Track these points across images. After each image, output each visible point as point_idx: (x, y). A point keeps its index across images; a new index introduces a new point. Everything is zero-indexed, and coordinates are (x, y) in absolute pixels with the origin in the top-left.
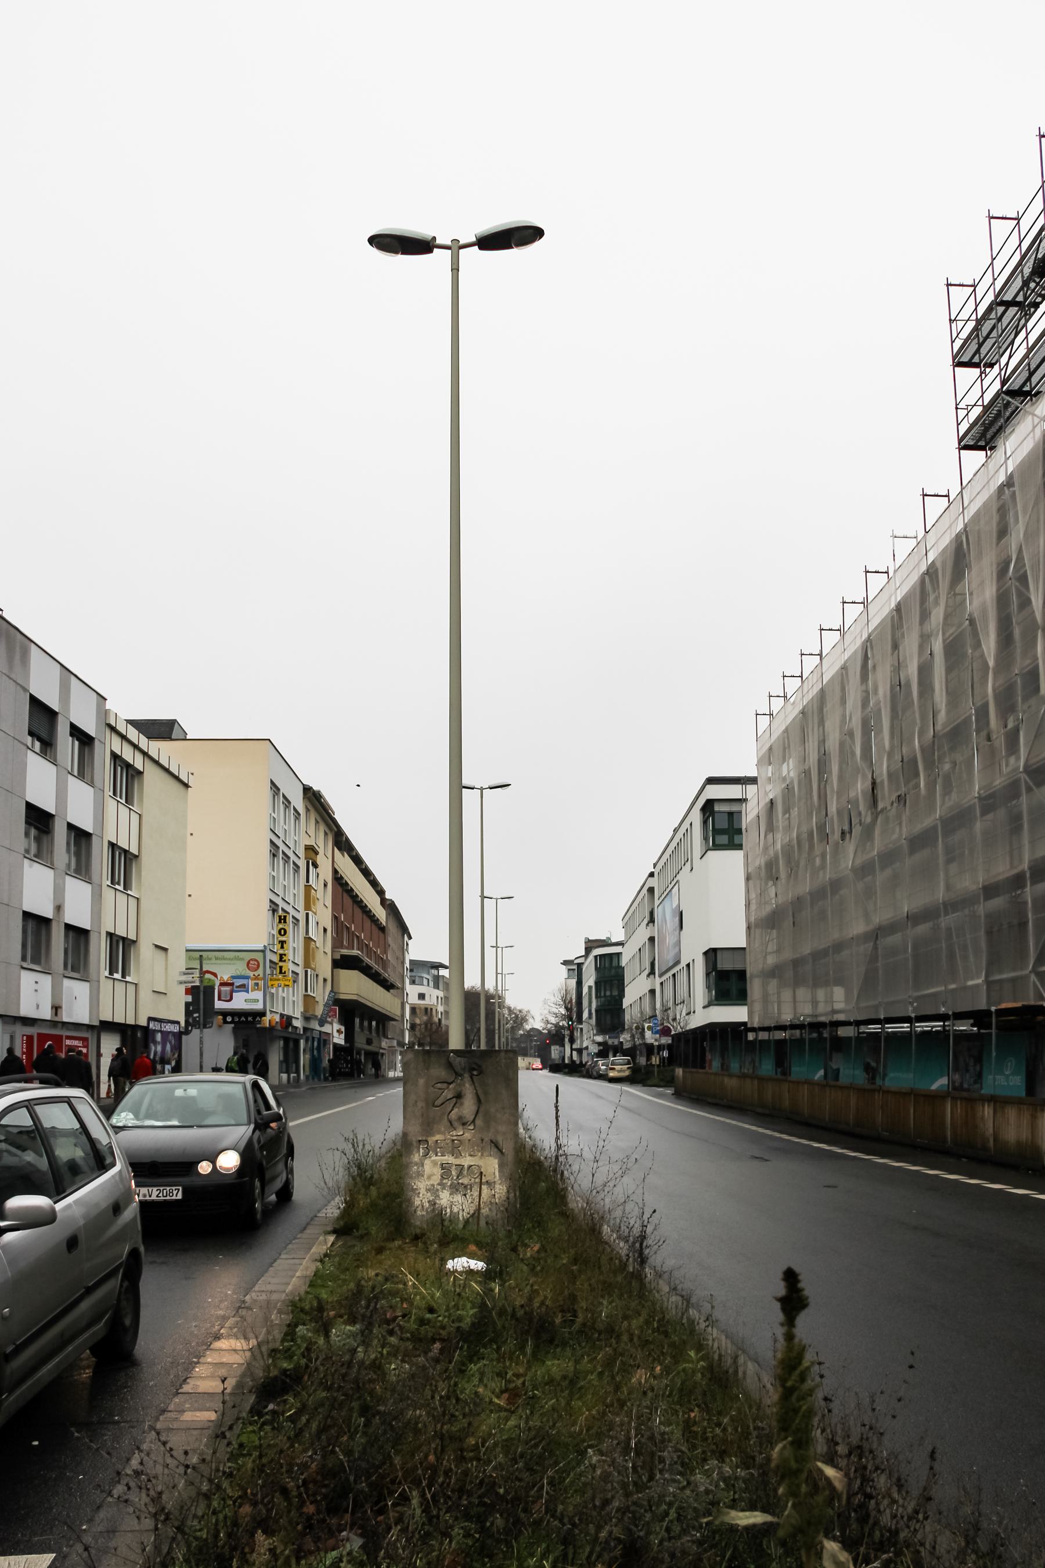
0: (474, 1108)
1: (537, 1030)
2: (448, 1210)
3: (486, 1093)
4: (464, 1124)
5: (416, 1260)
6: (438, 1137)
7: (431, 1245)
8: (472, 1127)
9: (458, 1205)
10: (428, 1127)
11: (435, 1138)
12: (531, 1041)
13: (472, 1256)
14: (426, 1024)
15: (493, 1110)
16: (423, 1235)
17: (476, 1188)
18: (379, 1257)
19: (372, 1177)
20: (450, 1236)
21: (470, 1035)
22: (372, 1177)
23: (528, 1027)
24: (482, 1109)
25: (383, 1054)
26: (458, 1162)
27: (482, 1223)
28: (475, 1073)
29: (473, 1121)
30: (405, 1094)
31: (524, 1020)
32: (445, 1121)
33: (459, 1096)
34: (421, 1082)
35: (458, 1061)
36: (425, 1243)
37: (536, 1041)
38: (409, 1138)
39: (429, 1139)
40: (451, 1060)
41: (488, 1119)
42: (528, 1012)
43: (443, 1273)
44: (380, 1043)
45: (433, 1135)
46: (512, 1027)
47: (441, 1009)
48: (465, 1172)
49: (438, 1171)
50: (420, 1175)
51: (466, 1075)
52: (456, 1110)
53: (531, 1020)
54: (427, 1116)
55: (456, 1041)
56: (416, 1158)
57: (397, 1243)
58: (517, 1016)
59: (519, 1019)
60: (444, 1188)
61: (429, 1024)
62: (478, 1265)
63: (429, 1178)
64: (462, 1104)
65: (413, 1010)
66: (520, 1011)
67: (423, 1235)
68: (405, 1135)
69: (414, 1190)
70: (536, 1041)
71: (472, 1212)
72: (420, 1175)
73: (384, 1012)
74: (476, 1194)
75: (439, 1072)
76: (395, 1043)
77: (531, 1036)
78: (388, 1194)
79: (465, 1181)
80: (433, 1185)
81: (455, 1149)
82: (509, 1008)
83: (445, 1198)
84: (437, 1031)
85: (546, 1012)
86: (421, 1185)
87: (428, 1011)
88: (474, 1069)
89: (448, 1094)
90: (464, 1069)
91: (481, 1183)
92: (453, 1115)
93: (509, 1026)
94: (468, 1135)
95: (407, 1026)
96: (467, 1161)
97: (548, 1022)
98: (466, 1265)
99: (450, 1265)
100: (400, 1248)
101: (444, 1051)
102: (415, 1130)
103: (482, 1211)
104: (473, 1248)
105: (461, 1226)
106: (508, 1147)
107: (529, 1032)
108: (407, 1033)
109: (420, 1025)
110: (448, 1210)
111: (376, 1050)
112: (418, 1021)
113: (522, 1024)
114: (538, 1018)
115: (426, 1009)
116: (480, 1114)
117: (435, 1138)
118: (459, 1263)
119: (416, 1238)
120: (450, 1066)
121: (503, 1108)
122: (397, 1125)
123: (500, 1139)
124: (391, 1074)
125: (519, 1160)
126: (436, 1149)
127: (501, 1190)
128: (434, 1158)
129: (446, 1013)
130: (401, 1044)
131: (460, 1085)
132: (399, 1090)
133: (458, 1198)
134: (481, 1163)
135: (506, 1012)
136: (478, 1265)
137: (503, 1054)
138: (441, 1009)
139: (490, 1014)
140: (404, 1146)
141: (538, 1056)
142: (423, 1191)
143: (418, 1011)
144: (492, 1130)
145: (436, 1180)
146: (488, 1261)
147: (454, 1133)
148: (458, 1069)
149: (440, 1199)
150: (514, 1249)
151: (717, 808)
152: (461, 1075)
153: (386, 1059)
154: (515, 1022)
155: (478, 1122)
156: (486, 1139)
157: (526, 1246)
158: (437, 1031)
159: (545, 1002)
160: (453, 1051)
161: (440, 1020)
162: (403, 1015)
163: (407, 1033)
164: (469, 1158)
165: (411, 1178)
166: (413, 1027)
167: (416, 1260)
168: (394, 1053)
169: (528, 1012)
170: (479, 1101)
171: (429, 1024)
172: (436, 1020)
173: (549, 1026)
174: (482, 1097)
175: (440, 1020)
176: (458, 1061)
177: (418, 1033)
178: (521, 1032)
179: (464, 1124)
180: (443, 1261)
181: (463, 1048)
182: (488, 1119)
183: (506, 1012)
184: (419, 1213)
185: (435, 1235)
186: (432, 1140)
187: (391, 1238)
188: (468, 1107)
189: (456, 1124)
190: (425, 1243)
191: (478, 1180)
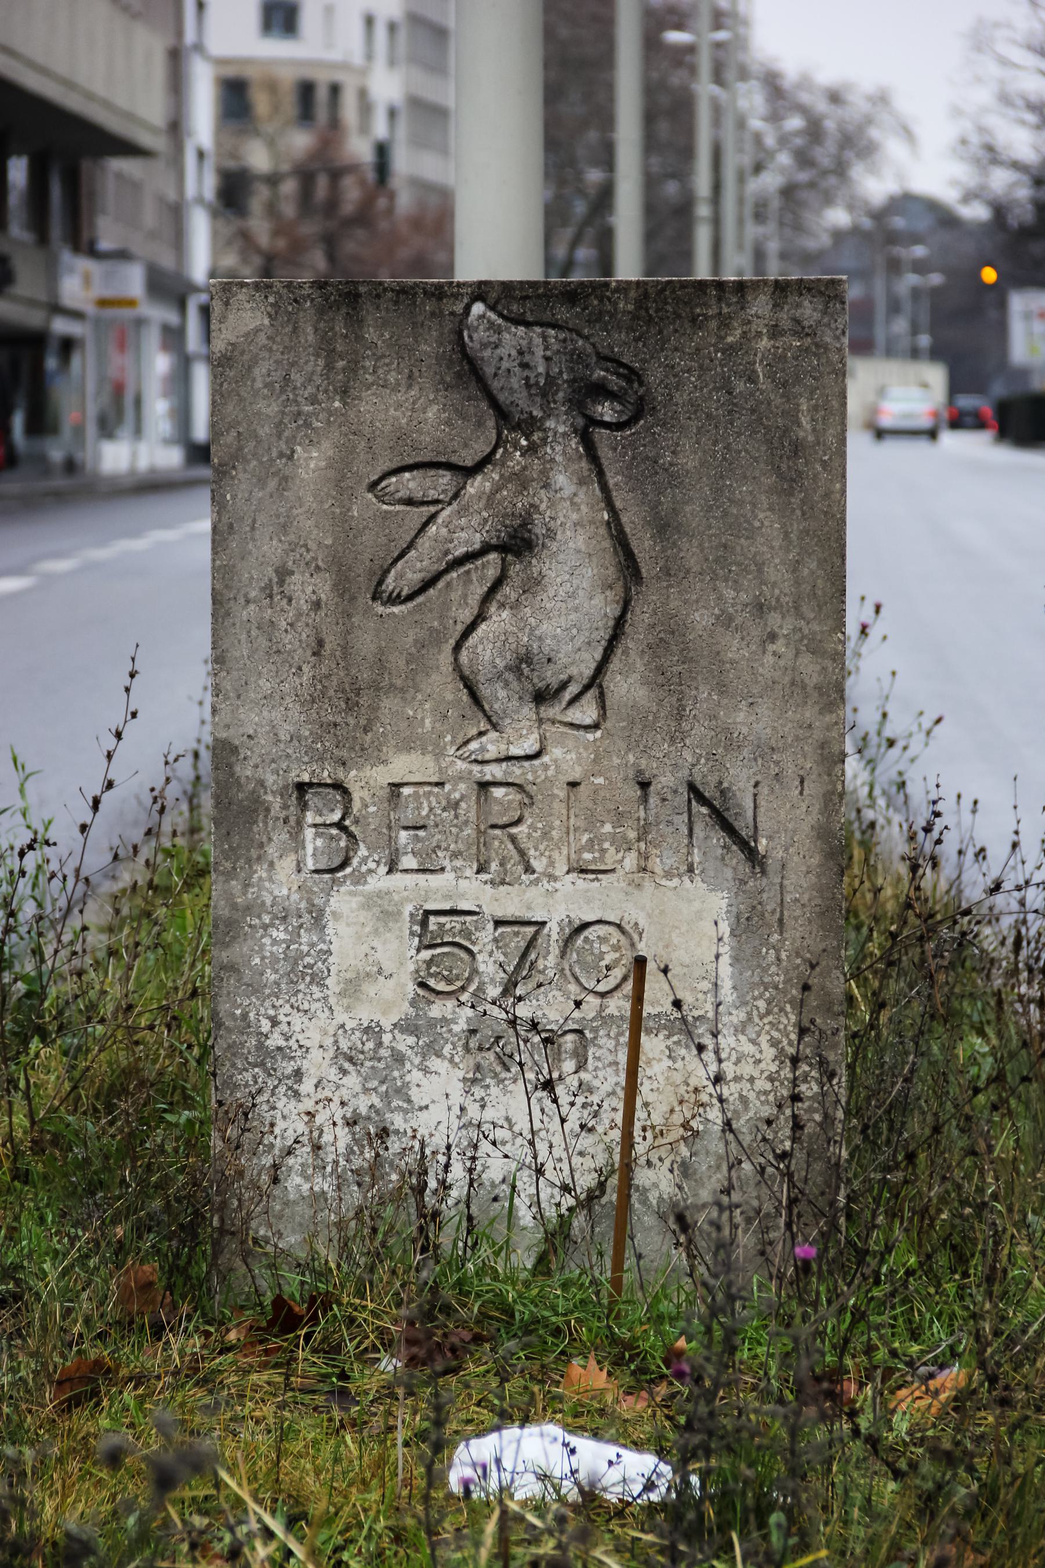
0: (602, 608)
1: (933, 207)
2: (458, 1172)
3: (664, 527)
4: (541, 697)
5: (284, 1434)
6: (402, 766)
7: (366, 1357)
8: (586, 712)
9: (511, 1144)
10: (349, 704)
11: (381, 776)
12: (894, 267)
13: (589, 1420)
14: (306, 176)
15: (701, 619)
16: (321, 1303)
17: (608, 1051)
18: (81, 1421)
19: (36, 994)
20: (461, 1318)
21: (573, 202)
22: (36, 994)
23: (875, 186)
24: (641, 617)
25: (68, 346)
26: (510, 902)
27: (651, 1239)
28: (606, 411)
29: (595, 681)
30: (219, 537)
31: (856, 144)
32: (441, 683)
33: (517, 543)
34: (312, 461)
35: (510, 349)
36: (331, 1349)
37: (920, 267)
38: (244, 771)
39: (352, 778)
40: (477, 337)
41: (678, 665)
42: (882, 99)
43: (429, 1514)
44: (52, 273)
45: (376, 757)
46: (788, 192)
47: (387, 86)
48: (549, 962)
49: (400, 955)
50: (305, 973)
51: (558, 425)
52: (499, 619)
53: (894, 148)
54: (349, 637)
55: (496, 238)
56: (281, 879)
57: (184, 1345)
58: (814, 131)
59: (828, 141)
60: (432, 1049)
61: (320, 171)
62: (628, 1470)
63: (352, 988)
64: (533, 585)
65: (236, 95)
66: (835, 97)
67: (321, 1303)
68: (224, 752)
69: (265, 1058)
70: (920, 267)
71: (586, 1181)
72: (305, 973)
73: (73, 102)
74: (607, 1080)
75: (405, 407)
76: (133, 281)
77: (892, 238)
78: (123, 1083)
79: (551, 1008)
80: (372, 1031)
81: (496, 839)
82: (773, 85)
83: (437, 1102)
84: (364, 217)
85: (984, 96)
86: (311, 1031)
87: (312, 99)
88: (601, 391)
89: (462, 529)
90: (545, 392)
91: (637, 1023)
92: (486, 650)
93: (770, 181)
94: (566, 757)
95: (200, 183)
96: (558, 900)
97: (991, 155)
98: (559, 1465)
99: (469, 1458)
100: (193, 1372)
101: (439, 293)
102: (276, 730)
103: (642, 1177)
104: (589, 1376)
105: (525, 1259)
106: (786, 828)
107: (880, 215)
108: (200, 230)
109: (273, 180)
110: (458, 1172)
111: (34, 319)
112: (258, 158)
113: (841, 170)
114: (938, 133)
115: (306, 90)
116: (633, 643)
117: (381, 776)
118: (526, 1458)
119: (284, 1318)
120: (468, 371)
121: (760, 608)
122: (177, 713)
123: (740, 778)
124: (115, 457)
125: (841, 911)
126: (402, 829)
127: (752, 1060)
128: (380, 881)
129: (428, 116)
130: (170, 288)
131: (521, 481)
132: (184, 534)
133: (510, 1102)
134: (633, 910)
135: (751, 100)
136: (628, 1470)
137: (760, 306)
138: (387, 86)
139: (670, 115)
140: (222, 809)
141: (936, 354)
142: (317, 1064)
143: (261, 102)
144: (699, 731)
145: (390, 999)
146: (687, 1439)
147: (492, 745)
148: (513, 390)
149: (410, 1108)
150: (826, 1390)
151: (200, 432)
152: (529, 425)
153: (84, 366)
154: (803, 159)
155: (626, 685)
156: (665, 780)
157: (888, 1378)
158: (364, 217)
159: (980, 39)
160: (481, 291)
161: (382, 151)
162: (176, 128)
163: (200, 230)
164: (569, 884)
165: (255, 989)
166: (233, 191)
167: (284, 1434)
168: (126, 336)
169: (882, 99)
170: (629, 567)
171: (320, 171)
172: (359, 149)
173: (1000, 180)
174: (643, 544)
175: (382, 151)
176: (510, 349)
177: (260, 227)
178: (838, 217)
179: (541, 697)
180: (436, 1445)
181: (536, 274)
182: (678, 665)
183: (751, 100)
184: (295, 1183)
185: (381, 1311)
186: (367, 782)
187: (143, 1318)
188: (567, 601)
189: (498, 696)
190: (331, 1349)
191: (619, 1005)
